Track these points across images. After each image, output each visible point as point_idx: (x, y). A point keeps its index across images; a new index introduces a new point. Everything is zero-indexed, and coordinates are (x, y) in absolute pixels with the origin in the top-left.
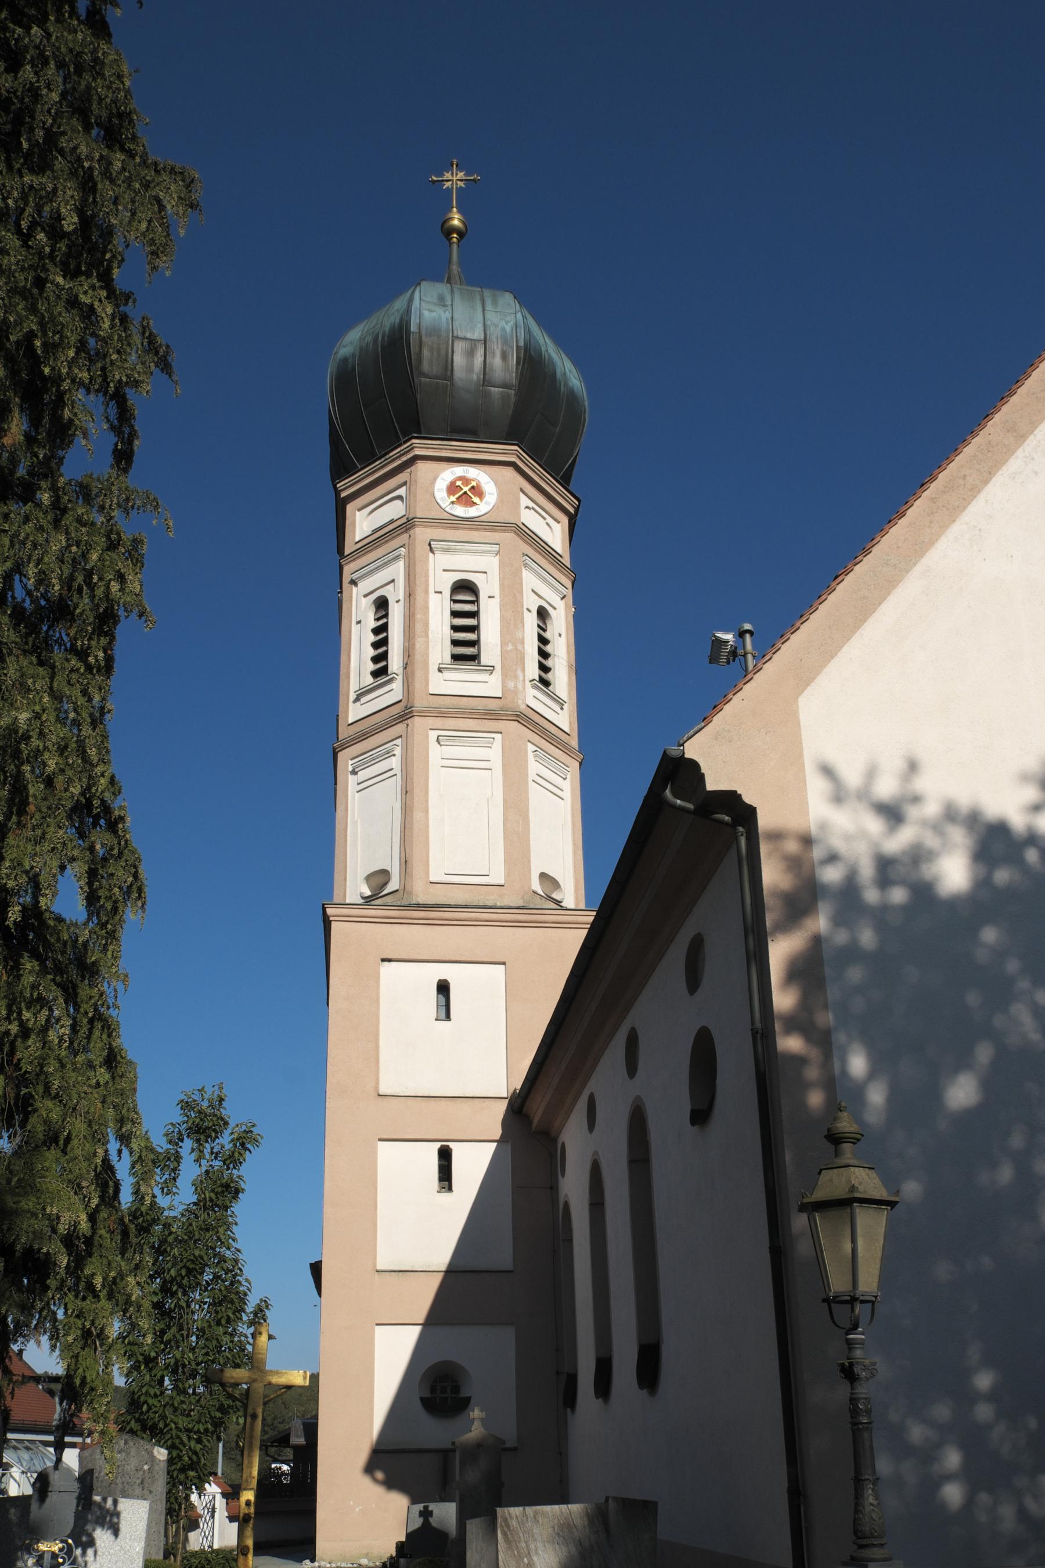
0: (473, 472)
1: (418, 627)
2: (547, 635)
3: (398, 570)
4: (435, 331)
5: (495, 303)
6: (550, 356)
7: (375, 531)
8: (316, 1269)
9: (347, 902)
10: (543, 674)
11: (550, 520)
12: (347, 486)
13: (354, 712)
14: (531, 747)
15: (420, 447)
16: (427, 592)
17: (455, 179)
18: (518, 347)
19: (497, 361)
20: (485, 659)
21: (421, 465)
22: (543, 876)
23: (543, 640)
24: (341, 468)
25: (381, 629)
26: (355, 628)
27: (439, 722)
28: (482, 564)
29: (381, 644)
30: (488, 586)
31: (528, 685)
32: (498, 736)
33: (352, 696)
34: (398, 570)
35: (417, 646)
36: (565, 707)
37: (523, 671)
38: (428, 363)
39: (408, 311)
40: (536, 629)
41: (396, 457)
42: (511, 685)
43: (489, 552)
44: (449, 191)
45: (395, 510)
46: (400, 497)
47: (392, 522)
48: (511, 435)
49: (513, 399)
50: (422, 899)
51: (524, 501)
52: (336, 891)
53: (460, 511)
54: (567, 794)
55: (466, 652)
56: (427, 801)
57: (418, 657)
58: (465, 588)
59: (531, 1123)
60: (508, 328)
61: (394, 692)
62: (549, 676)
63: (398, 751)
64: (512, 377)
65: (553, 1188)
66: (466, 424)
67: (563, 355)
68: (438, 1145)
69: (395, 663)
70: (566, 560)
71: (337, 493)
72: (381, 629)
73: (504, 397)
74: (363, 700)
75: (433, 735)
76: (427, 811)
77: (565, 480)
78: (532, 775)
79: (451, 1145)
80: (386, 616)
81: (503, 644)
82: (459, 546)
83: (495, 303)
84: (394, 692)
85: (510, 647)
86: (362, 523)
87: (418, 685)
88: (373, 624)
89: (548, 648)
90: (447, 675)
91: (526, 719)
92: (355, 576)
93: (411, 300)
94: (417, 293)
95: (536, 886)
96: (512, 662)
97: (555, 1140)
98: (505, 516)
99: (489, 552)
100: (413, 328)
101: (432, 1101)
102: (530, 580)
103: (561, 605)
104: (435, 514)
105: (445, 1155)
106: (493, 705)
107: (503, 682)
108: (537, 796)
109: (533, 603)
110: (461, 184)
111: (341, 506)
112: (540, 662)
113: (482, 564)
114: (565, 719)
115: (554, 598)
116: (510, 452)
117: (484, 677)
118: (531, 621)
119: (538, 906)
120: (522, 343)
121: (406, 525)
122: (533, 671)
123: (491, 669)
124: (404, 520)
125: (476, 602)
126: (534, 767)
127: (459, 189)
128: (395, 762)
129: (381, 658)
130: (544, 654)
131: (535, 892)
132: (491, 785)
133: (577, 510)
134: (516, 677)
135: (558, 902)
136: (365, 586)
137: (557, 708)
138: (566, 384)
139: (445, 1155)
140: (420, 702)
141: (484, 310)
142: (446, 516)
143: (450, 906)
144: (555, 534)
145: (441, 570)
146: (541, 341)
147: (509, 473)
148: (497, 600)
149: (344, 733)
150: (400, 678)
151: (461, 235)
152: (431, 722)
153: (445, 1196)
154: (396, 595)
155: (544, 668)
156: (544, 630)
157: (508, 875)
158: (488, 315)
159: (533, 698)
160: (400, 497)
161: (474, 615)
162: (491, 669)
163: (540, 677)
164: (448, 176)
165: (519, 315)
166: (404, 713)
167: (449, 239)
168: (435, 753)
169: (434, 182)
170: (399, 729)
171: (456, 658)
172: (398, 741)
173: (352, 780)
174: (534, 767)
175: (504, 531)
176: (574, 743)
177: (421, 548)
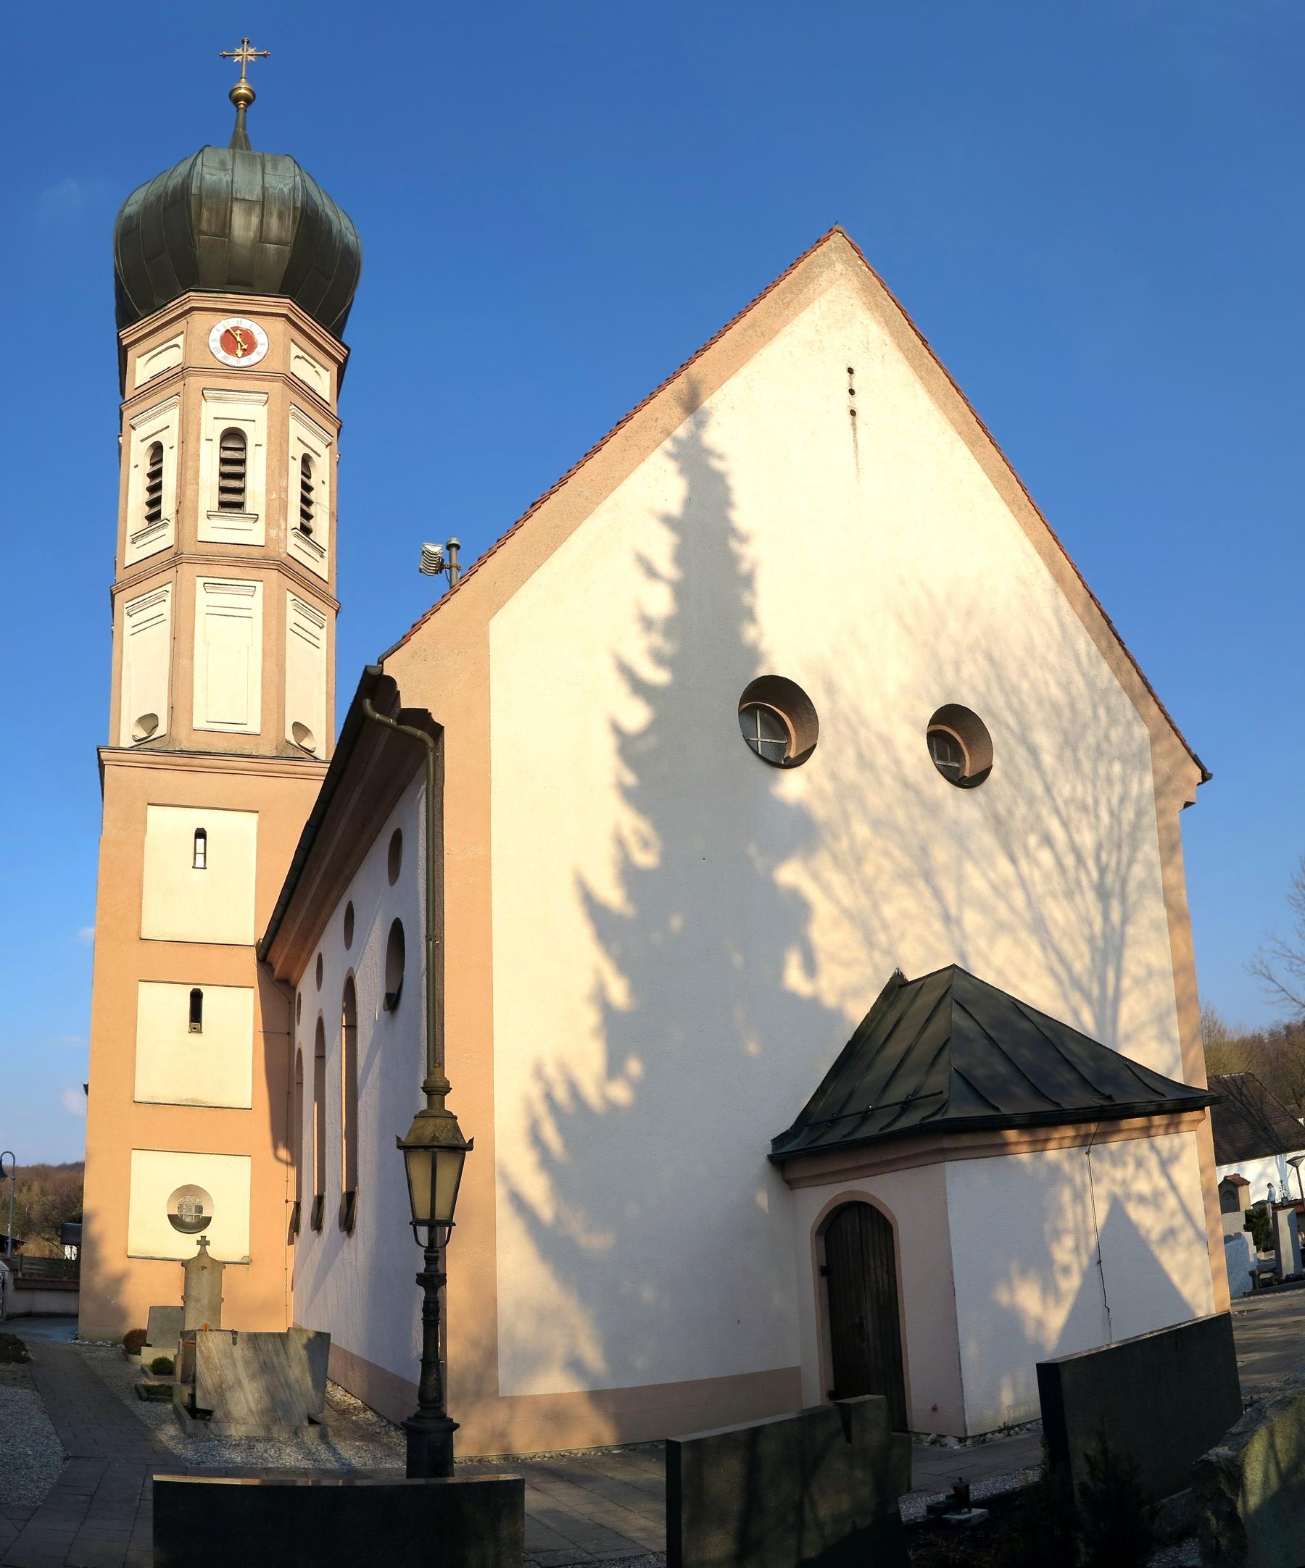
0: (245, 323)
1: (190, 474)
2: (312, 482)
3: (171, 417)
4: (215, 193)
5: (275, 167)
6: (327, 216)
7: (153, 378)
8: (86, 1087)
9: (122, 745)
10: (305, 522)
11: (319, 368)
12: (129, 335)
13: (132, 554)
14: (290, 596)
15: (195, 299)
16: (198, 440)
17: (245, 54)
18: (295, 208)
19: (274, 222)
20: (249, 508)
21: (197, 316)
22: (298, 727)
23: (306, 487)
24: (126, 317)
25: (156, 475)
26: (133, 471)
27: (205, 569)
28: (253, 415)
29: (155, 488)
30: (256, 435)
31: (290, 532)
32: (259, 585)
33: (129, 539)
34: (171, 417)
35: (188, 492)
36: (326, 554)
37: (286, 520)
38: (206, 221)
39: (189, 175)
40: (300, 476)
41: (175, 307)
42: (273, 533)
43: (258, 401)
44: (239, 64)
45: (171, 358)
46: (177, 346)
47: (169, 369)
48: (285, 289)
49: (288, 255)
50: (185, 746)
51: (295, 351)
52: (112, 733)
53: (232, 361)
54: (323, 643)
55: (232, 499)
56: (193, 648)
57: (188, 503)
58: (233, 436)
59: (273, 970)
60: (286, 190)
61: (165, 537)
62: (312, 524)
63: (169, 597)
64: (289, 235)
65: (290, 1034)
66: (240, 278)
67: (377, 1060)
68: (191, 988)
69: (168, 508)
70: (334, 409)
71: (119, 340)
72: (156, 475)
73: (278, 253)
74: (139, 544)
75: (200, 581)
76: (192, 658)
77: (337, 332)
78: (290, 625)
79: (203, 989)
80: (161, 461)
81: (268, 491)
82: (230, 395)
83: (275, 167)
84: (165, 537)
85: (274, 496)
86: (143, 369)
87: (187, 531)
88: (149, 469)
89: (312, 496)
90: (215, 522)
91: (288, 568)
92: (133, 422)
93: (193, 165)
94: (200, 159)
95: (289, 736)
96: (277, 508)
97: (294, 988)
98: (276, 366)
99: (258, 401)
100: (194, 190)
101: (187, 948)
102: (296, 429)
103: (325, 452)
104: (209, 363)
105: (196, 997)
106: (256, 553)
107: (267, 531)
108: (294, 644)
109: (297, 451)
110: (252, 58)
111: (123, 353)
112: (302, 510)
113: (253, 415)
114: (322, 567)
115: (319, 446)
116: (283, 305)
117: (248, 525)
118: (295, 468)
119: (293, 753)
120: (299, 204)
121: (182, 372)
122: (295, 519)
123: (256, 518)
124: (179, 369)
125: (243, 449)
126: (292, 616)
127: (249, 64)
128: (165, 608)
129: (155, 503)
130: (306, 501)
131: (288, 742)
132: (251, 633)
133: (346, 359)
134: (279, 526)
135: (309, 752)
136: (143, 431)
137: (317, 556)
138: (341, 239)
139: (196, 997)
140: (188, 549)
141: (263, 173)
142: (219, 365)
143: (209, 754)
144: (322, 382)
145: (215, 416)
146: (319, 202)
147: (280, 324)
148: (264, 448)
149: (121, 575)
150: (172, 524)
151: (249, 101)
152: (199, 569)
153: (195, 1036)
154: (170, 441)
155: (306, 516)
156: (309, 477)
157: (263, 724)
158: (267, 178)
159: (294, 547)
160: (177, 346)
161: (242, 462)
162: (256, 518)
163: (302, 525)
164: (239, 51)
165: (298, 179)
166: (174, 558)
167: (237, 105)
168: (203, 599)
169: (224, 56)
170: (170, 574)
171: (223, 504)
172: (169, 587)
173: (128, 622)
174: (292, 616)
175: (273, 381)
176: (332, 591)
177: (194, 396)
